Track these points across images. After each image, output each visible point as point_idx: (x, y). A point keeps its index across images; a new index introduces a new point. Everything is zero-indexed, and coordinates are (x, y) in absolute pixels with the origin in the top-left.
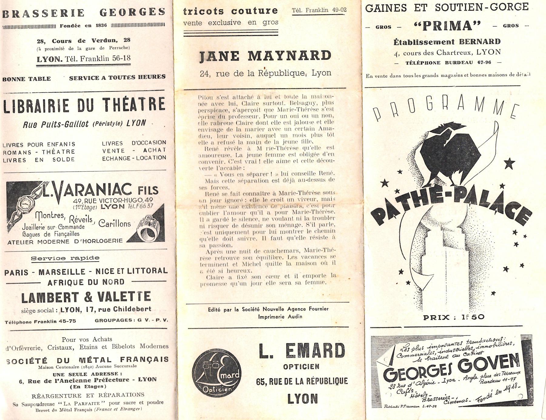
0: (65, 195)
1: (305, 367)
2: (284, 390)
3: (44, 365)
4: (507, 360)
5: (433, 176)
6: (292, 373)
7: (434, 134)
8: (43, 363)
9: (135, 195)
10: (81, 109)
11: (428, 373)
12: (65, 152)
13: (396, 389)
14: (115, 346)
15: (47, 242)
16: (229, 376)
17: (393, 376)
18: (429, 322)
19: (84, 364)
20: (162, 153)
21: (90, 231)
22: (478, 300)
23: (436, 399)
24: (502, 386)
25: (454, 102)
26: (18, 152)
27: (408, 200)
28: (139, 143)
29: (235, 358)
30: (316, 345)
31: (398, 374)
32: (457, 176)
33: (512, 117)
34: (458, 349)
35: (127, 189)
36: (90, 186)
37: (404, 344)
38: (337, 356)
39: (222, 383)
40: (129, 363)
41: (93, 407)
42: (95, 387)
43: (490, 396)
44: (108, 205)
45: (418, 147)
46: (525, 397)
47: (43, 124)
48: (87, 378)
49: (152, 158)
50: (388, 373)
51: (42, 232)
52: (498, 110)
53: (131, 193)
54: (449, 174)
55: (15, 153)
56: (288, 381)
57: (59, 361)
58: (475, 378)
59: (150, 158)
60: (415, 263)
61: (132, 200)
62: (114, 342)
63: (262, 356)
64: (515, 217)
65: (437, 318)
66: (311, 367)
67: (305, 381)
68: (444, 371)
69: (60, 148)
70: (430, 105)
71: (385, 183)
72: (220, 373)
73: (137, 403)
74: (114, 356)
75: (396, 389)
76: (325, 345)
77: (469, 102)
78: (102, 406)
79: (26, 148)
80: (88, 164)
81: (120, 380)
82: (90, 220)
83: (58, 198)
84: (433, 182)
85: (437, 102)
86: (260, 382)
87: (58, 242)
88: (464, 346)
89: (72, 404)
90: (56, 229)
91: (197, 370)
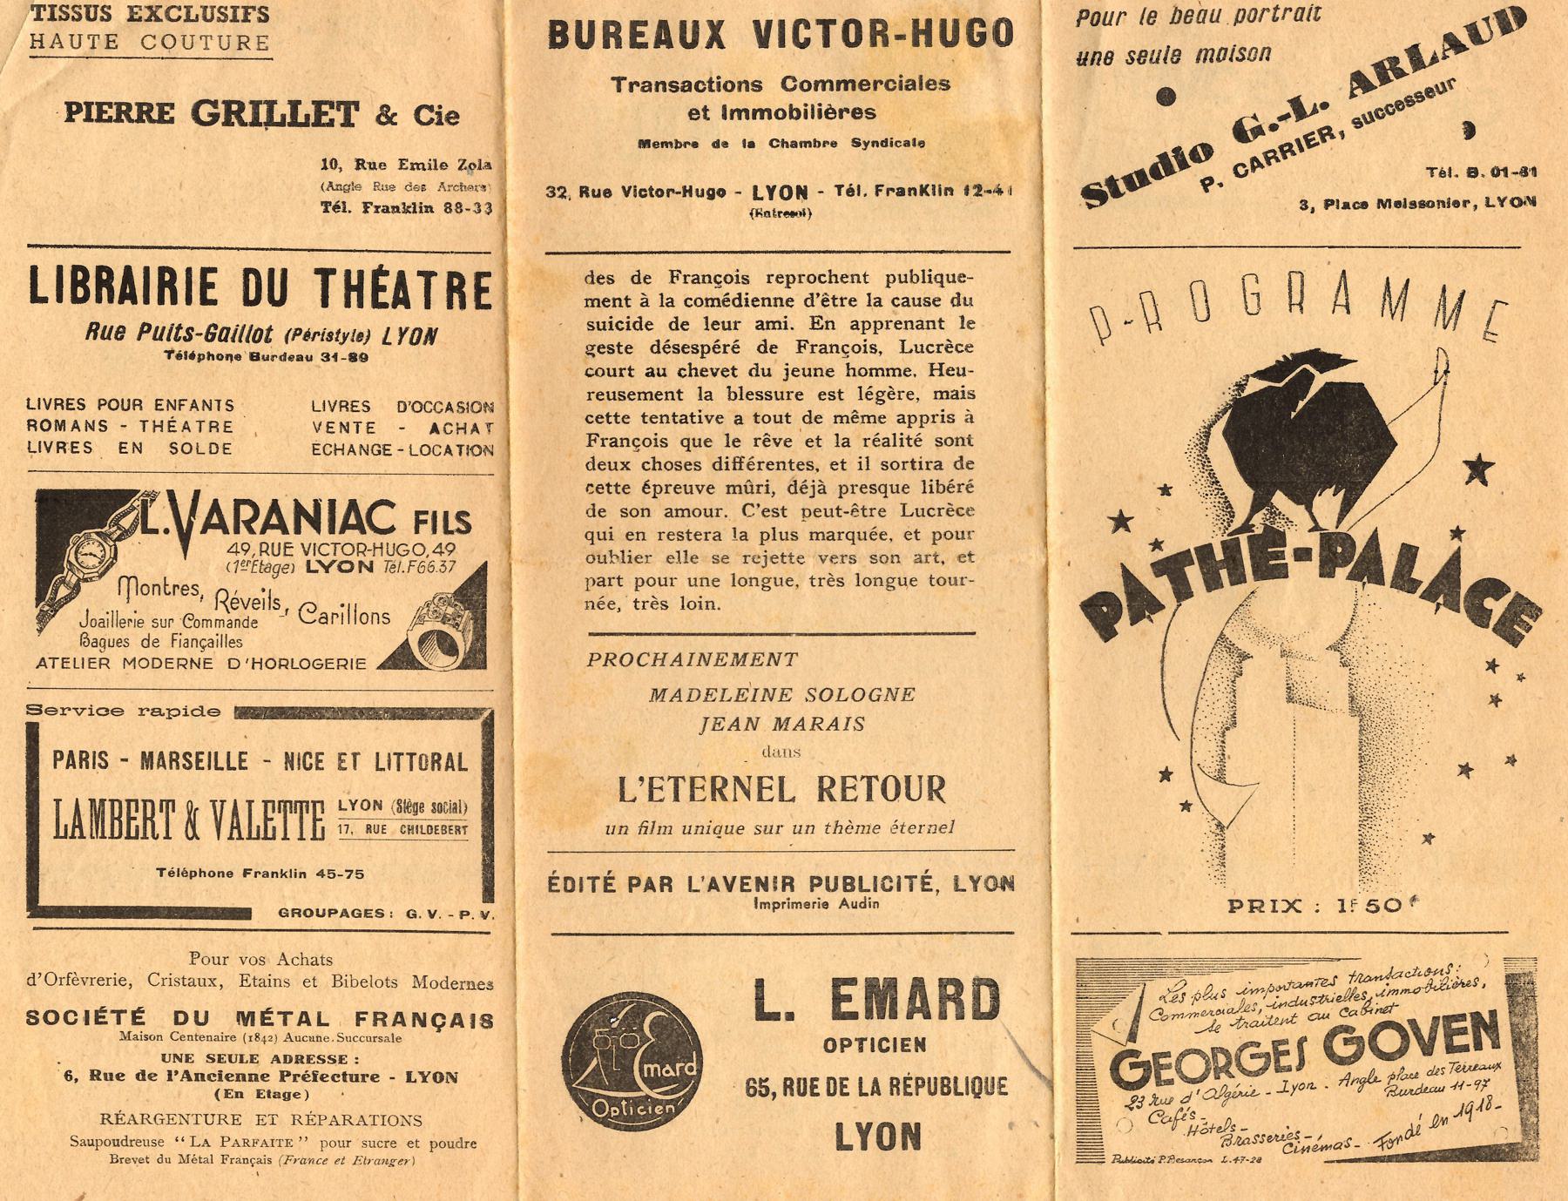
0: (204, 531)
1: (885, 1045)
2: (825, 1111)
3: (136, 1030)
4: (1463, 1031)
5: (1261, 502)
6: (848, 1064)
7: (1264, 384)
8: (134, 1023)
9: (404, 533)
10: (252, 296)
11: (1239, 1065)
12: (206, 427)
13: (1148, 1109)
14: (338, 981)
15: (154, 664)
16: (668, 1071)
17: (1137, 1074)
18: (1243, 919)
19: (250, 1030)
20: (481, 439)
21: (271, 634)
22: (1385, 857)
23: (1262, 1138)
24: (1449, 1103)
25: (1321, 290)
26: (69, 426)
27: (1187, 569)
28: (417, 407)
29: (684, 1018)
30: (918, 985)
31: (1152, 1069)
32: (1327, 503)
33: (1489, 336)
34: (1323, 999)
35: (382, 517)
36: (275, 507)
37: (1169, 983)
38: (978, 1015)
39: (646, 1090)
40: (380, 1030)
41: (273, 1153)
42: (287, 1097)
43: (1413, 1133)
44: (326, 561)
45: (1218, 417)
46: (1515, 1136)
47: (142, 332)
48: (257, 1070)
49: (455, 450)
50: (1124, 1066)
51: (135, 635)
52: (1450, 310)
53: (392, 529)
54: (1304, 498)
55: (61, 425)
56: (837, 1087)
57: (179, 1017)
58: (1372, 1079)
59: (449, 450)
60: (1206, 752)
61: (396, 548)
62: (340, 967)
63: (762, 1015)
64: (1492, 624)
65: (1268, 907)
66: (903, 1045)
67: (884, 1086)
68: (1284, 1061)
69: (192, 417)
70: (1252, 301)
71: (1121, 522)
72: (641, 1064)
73: (402, 1144)
74: (338, 1007)
75: (1148, 1109)
76: (943, 983)
77: (1365, 294)
78: (298, 1151)
79: (92, 413)
80: (271, 438)
81: (355, 1078)
82: (275, 604)
83: (185, 538)
84: (1258, 520)
85: (1274, 291)
86: (757, 1088)
87: (183, 664)
88: (1342, 987)
89: (215, 1141)
90: (177, 626)
91: (579, 1048)
